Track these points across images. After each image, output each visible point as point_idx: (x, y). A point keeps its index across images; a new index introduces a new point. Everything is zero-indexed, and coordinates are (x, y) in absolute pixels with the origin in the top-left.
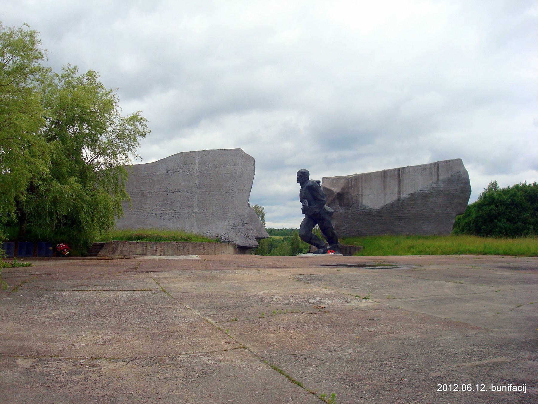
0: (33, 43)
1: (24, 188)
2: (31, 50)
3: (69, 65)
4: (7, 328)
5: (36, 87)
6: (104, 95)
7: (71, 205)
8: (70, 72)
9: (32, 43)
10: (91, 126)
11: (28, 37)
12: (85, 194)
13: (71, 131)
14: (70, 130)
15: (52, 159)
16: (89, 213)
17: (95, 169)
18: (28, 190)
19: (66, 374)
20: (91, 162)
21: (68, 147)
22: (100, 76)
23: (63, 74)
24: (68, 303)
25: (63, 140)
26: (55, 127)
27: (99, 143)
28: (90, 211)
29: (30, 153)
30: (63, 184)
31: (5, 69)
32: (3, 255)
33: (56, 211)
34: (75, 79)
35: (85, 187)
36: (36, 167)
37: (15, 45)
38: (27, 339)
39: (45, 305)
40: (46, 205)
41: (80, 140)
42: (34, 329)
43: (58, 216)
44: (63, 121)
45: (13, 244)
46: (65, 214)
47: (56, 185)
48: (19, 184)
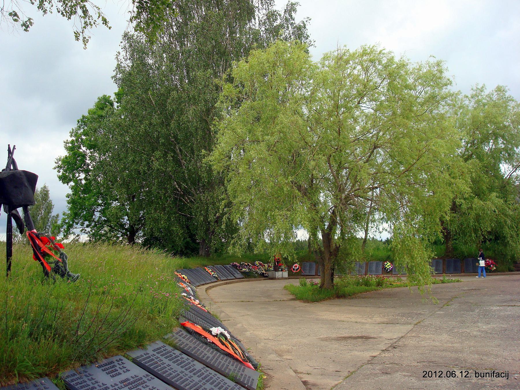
0: (441, 72)
1: (447, 208)
2: (440, 78)
3: (477, 84)
4: (441, 341)
5: (448, 111)
6: (516, 107)
7: (494, 221)
8: (478, 91)
9: (439, 72)
10: (506, 140)
11: (435, 67)
12: (507, 209)
13: (487, 148)
14: (486, 147)
15: (472, 178)
16: (513, 227)
17: (514, 182)
18: (452, 209)
19: (501, 387)
20: (510, 175)
21: (486, 164)
22: (509, 89)
23: (473, 94)
24: (498, 318)
25: (480, 158)
26: (471, 147)
27: (516, 156)
28: (513, 225)
29: (450, 175)
30: (484, 201)
31: (419, 100)
32: (432, 272)
33: (480, 228)
34: (484, 96)
35: (506, 201)
36: (458, 187)
37: (425, 77)
38: (461, 352)
39: (476, 320)
40: (469, 222)
41: (496, 155)
42: (467, 342)
43: (482, 232)
44: (478, 139)
45: (441, 261)
46: (489, 230)
47: (477, 203)
48: (443, 205)
